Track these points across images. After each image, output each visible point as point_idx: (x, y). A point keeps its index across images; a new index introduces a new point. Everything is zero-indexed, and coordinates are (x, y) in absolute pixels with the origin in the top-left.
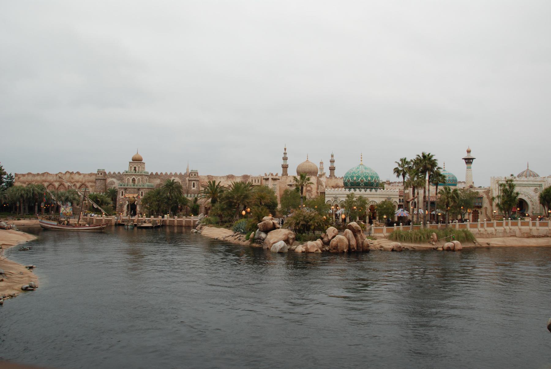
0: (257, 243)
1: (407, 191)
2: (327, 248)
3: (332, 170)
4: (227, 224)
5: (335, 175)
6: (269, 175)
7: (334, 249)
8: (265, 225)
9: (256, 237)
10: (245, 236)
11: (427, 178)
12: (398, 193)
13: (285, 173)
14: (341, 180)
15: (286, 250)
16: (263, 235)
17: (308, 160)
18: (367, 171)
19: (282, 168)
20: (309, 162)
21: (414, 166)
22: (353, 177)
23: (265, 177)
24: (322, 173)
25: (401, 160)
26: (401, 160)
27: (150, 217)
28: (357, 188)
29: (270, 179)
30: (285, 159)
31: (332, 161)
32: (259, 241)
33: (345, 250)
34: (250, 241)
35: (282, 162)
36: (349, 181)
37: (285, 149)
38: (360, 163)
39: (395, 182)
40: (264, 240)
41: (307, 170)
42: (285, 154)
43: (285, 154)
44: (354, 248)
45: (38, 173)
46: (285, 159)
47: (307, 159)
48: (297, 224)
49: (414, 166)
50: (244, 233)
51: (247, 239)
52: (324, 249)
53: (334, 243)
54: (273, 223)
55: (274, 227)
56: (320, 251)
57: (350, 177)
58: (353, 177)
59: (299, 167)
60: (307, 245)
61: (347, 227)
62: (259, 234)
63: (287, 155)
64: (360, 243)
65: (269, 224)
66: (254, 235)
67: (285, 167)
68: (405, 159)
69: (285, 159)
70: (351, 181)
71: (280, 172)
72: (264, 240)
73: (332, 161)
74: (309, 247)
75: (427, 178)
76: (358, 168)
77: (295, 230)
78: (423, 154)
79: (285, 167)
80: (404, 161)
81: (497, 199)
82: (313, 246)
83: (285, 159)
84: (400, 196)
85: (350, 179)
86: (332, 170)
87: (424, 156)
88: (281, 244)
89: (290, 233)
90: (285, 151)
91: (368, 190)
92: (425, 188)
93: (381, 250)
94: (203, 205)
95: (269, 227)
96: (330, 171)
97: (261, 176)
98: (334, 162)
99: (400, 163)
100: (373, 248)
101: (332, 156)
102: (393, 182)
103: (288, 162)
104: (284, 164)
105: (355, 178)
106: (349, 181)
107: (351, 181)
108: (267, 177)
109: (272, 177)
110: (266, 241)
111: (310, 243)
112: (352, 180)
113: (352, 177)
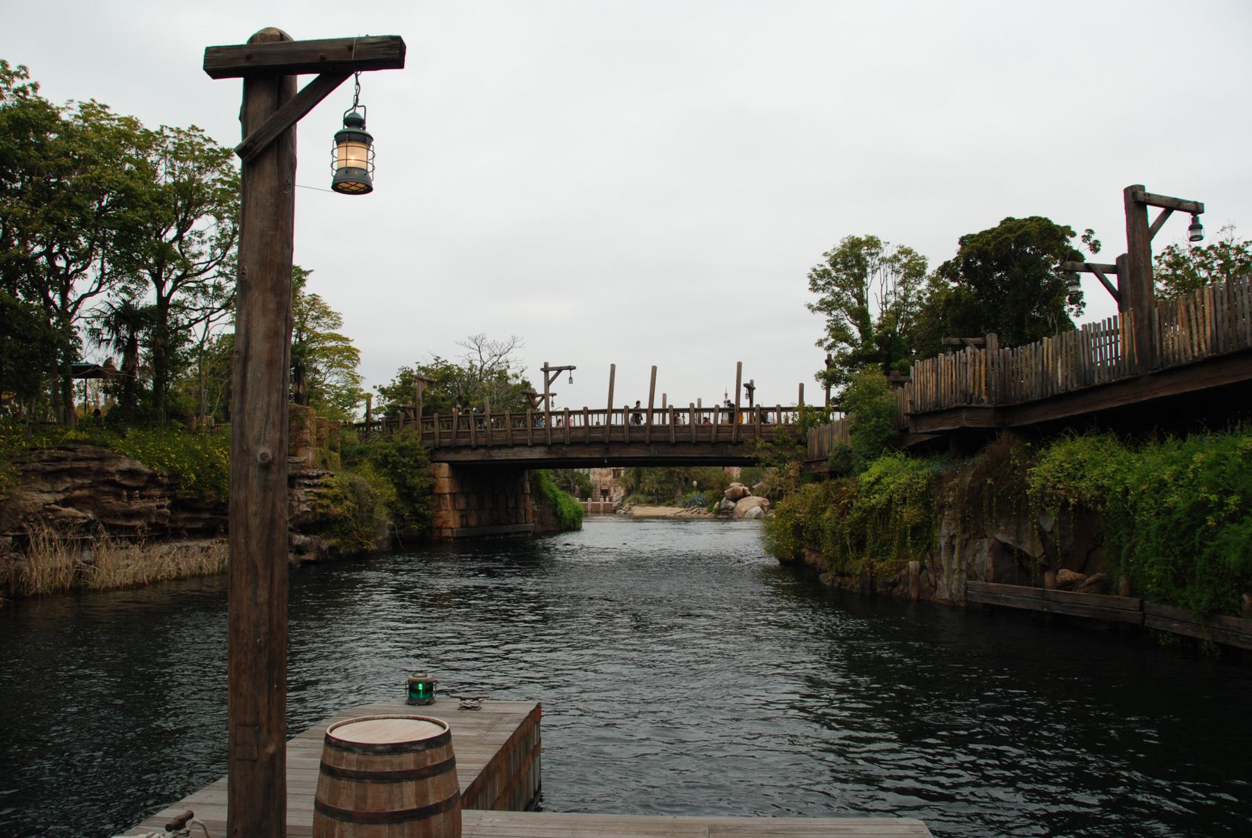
0: (724, 514)
4: (667, 502)
5: (303, 270)
8: (734, 492)
9: (722, 506)
10: (705, 509)
16: (732, 504)
21: (971, 746)
27: (586, 500)
40: (733, 509)
45: (960, 236)
48: (773, 490)
50: (703, 506)
51: (709, 512)
54: (744, 490)
55: (744, 495)
61: (329, 557)
62: (726, 503)
65: (738, 490)
66: (720, 505)
72: (733, 509)
77: (768, 497)
81: (621, 800)
88: (757, 509)
89: (763, 501)
94: (598, 487)
95: (739, 494)
110: (735, 510)
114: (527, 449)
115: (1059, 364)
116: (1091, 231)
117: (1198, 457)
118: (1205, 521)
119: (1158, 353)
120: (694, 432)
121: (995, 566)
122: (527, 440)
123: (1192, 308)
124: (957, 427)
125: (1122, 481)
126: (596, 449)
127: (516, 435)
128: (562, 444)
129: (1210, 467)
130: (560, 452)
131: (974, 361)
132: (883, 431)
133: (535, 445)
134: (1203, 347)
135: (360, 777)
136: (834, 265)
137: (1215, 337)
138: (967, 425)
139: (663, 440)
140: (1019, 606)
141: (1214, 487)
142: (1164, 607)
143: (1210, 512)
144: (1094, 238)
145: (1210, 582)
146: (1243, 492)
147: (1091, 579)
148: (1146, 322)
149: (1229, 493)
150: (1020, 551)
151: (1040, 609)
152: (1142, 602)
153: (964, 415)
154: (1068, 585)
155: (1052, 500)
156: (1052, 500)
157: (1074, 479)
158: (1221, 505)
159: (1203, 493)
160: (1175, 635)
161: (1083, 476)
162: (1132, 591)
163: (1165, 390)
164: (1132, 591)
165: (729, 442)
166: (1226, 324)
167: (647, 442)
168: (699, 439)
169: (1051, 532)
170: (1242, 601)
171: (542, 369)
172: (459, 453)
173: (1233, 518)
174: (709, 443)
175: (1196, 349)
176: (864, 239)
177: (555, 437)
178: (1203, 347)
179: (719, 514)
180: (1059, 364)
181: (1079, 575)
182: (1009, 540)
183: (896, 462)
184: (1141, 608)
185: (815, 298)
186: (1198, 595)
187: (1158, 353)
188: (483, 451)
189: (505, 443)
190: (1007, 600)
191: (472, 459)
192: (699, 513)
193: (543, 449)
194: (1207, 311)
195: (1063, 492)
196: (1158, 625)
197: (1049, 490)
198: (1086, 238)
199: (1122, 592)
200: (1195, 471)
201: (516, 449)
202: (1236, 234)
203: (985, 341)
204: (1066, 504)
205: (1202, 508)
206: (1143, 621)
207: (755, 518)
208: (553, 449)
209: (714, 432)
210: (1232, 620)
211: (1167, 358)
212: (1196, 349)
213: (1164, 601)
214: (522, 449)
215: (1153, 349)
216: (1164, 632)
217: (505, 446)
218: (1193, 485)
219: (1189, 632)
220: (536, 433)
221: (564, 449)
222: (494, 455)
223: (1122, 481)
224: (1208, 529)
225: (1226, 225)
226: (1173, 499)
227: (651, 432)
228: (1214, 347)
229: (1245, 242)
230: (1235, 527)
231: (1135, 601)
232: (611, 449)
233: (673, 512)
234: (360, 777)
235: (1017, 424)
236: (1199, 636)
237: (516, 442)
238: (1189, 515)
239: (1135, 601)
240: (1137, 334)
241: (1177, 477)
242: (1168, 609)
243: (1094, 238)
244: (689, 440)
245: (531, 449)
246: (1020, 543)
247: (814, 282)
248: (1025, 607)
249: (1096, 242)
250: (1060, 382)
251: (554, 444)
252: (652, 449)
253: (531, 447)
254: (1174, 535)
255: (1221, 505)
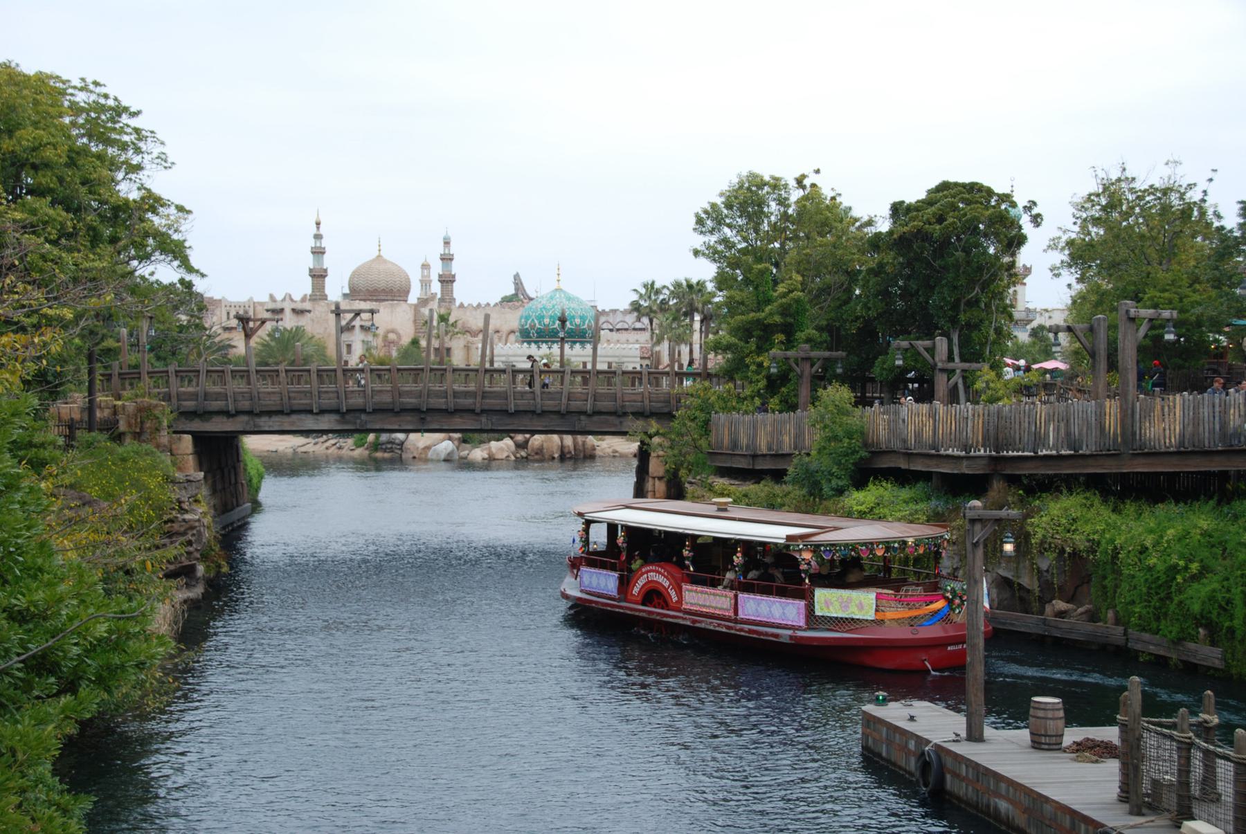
0: (385, 451)
1: (657, 349)
2: (523, 454)
3: (447, 282)
6: (284, 300)
7: (537, 454)
11: (697, 326)
12: (638, 353)
13: (318, 293)
14: (474, 313)
15: (456, 457)
17: (382, 253)
18: (572, 306)
19: (310, 279)
20: (385, 261)
22: (543, 317)
23: (271, 306)
24: (429, 293)
25: (645, 286)
26: (645, 286)
28: (543, 342)
29: (288, 312)
30: (318, 253)
31: (447, 259)
32: (389, 446)
33: (556, 455)
34: (367, 449)
35: (309, 261)
36: (533, 327)
37: (318, 224)
38: (555, 286)
39: (614, 311)
40: (402, 443)
41: (382, 285)
42: (318, 237)
43: (318, 237)
44: (570, 452)
46: (318, 252)
47: (377, 253)
49: (675, 599)
51: (358, 446)
52: (518, 455)
53: (536, 443)
56: (513, 458)
57: (536, 317)
58: (543, 317)
59: (355, 274)
60: (490, 448)
63: (323, 241)
64: (580, 443)
67: (318, 276)
68: (653, 283)
69: (318, 253)
70: (538, 326)
71: (304, 287)
72: (402, 443)
73: (447, 259)
74: (494, 450)
75: (697, 326)
76: (552, 298)
78: (687, 281)
79: (318, 276)
80: (651, 288)
82: (502, 449)
83: (318, 252)
84: (642, 358)
85: (536, 321)
86: (447, 282)
87: (690, 286)
90: (318, 228)
91: (578, 346)
92: (691, 345)
93: (614, 456)
96: (442, 287)
97: (255, 300)
98: (451, 260)
99: (643, 291)
100: (601, 454)
101: (447, 243)
102: (607, 310)
103: (327, 261)
104: (317, 267)
105: (547, 321)
106: (533, 327)
107: (538, 326)
108: (279, 306)
109: (294, 306)
110: (407, 445)
111: (494, 445)
112: (540, 324)
113: (541, 318)
114: (310, 416)
115: (1051, 429)
116: (1034, 203)
117: (1171, 532)
118: (1175, 578)
119: (1138, 437)
120: (538, 400)
121: (998, 597)
122: (311, 405)
123: (1166, 409)
124: (956, 472)
125: (1112, 541)
126: (409, 418)
127: (295, 399)
128: (363, 411)
129: (1180, 540)
130: (358, 421)
131: (974, 415)
132: (855, 452)
133: (323, 412)
134: (1173, 440)
135: (1053, 710)
136: (729, 206)
137: (1182, 435)
138: (967, 472)
139: (498, 408)
140: (1022, 630)
141: (1182, 556)
142: (1143, 634)
143: (1178, 572)
144: (1035, 211)
145: (1177, 620)
146: (1202, 561)
147: (1080, 610)
148: (1129, 412)
149: (1191, 561)
150: (1019, 584)
151: (1040, 632)
152: (1125, 630)
153: (965, 463)
154: (1061, 614)
155: (1050, 547)
156: (1050, 547)
157: (1069, 531)
158: (1186, 568)
159: (1174, 559)
160: (1150, 654)
161: (1076, 530)
162: (1118, 622)
163: (1141, 467)
164: (1118, 622)
165: (584, 413)
166: (1191, 426)
167: (478, 410)
168: (545, 408)
169: (1047, 571)
170: (1198, 633)
171: (332, 312)
172: (207, 420)
173: (1194, 578)
174: (558, 413)
175: (1167, 441)
176: (767, 178)
177: (351, 401)
178: (1173, 440)
179: (376, 450)
180: (1051, 429)
181: (1070, 606)
182: (1009, 575)
183: (887, 494)
184: (1125, 633)
185: (699, 241)
186: (1170, 628)
187: (1138, 437)
188: (245, 418)
189: (279, 408)
190: (1012, 625)
191: (229, 429)
192: (340, 448)
193: (334, 417)
194: (1177, 414)
195: (1059, 542)
196: (1138, 647)
197: (1049, 540)
198: (1028, 209)
199: (1110, 622)
200: (1168, 542)
201: (294, 417)
202: (1180, 170)
203: (934, 343)
204: (1063, 551)
205: (1174, 569)
206: (1127, 644)
207: (446, 460)
208: (348, 417)
209: (564, 400)
210: (1192, 645)
211: (1145, 444)
212: (1167, 441)
213: (1144, 630)
214: (303, 416)
215: (1134, 434)
216: (1143, 652)
217: (280, 412)
218: (1166, 553)
219: (1162, 653)
220: (323, 396)
221: (363, 417)
222: (262, 424)
223: (1112, 541)
224: (1178, 584)
225: (1171, 159)
226: (1152, 561)
227: (483, 397)
228: (1182, 443)
229: (1189, 185)
230: (1195, 585)
231: (1120, 629)
232: (428, 419)
233: (289, 445)
234: (1053, 710)
235: (1009, 472)
236: (1169, 655)
237: (295, 408)
238: (1165, 573)
239: (1120, 629)
240: (1122, 421)
241: (1156, 544)
242: (1146, 636)
243: (1035, 211)
244: (532, 409)
245: (316, 417)
246: (1019, 577)
247: (700, 221)
248: (1028, 631)
249: (1038, 215)
250: (1051, 443)
251: (349, 411)
252: (484, 419)
253: (317, 414)
254: (1153, 586)
255: (1186, 568)
